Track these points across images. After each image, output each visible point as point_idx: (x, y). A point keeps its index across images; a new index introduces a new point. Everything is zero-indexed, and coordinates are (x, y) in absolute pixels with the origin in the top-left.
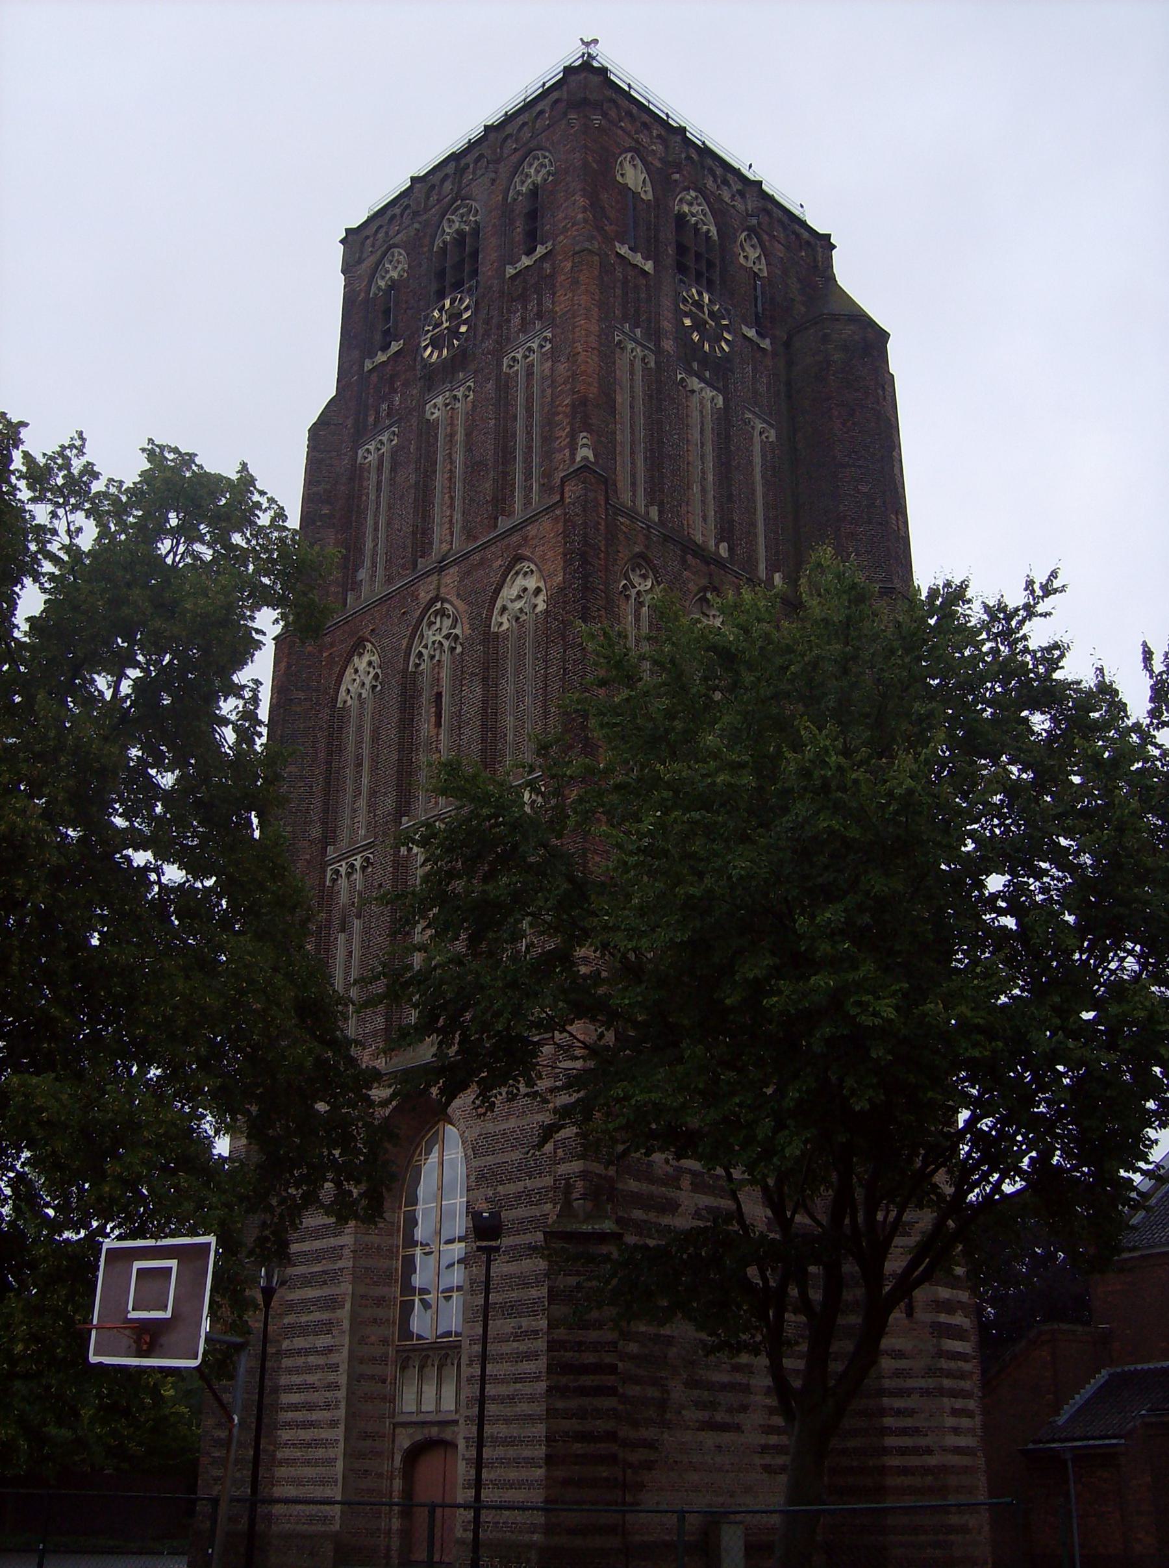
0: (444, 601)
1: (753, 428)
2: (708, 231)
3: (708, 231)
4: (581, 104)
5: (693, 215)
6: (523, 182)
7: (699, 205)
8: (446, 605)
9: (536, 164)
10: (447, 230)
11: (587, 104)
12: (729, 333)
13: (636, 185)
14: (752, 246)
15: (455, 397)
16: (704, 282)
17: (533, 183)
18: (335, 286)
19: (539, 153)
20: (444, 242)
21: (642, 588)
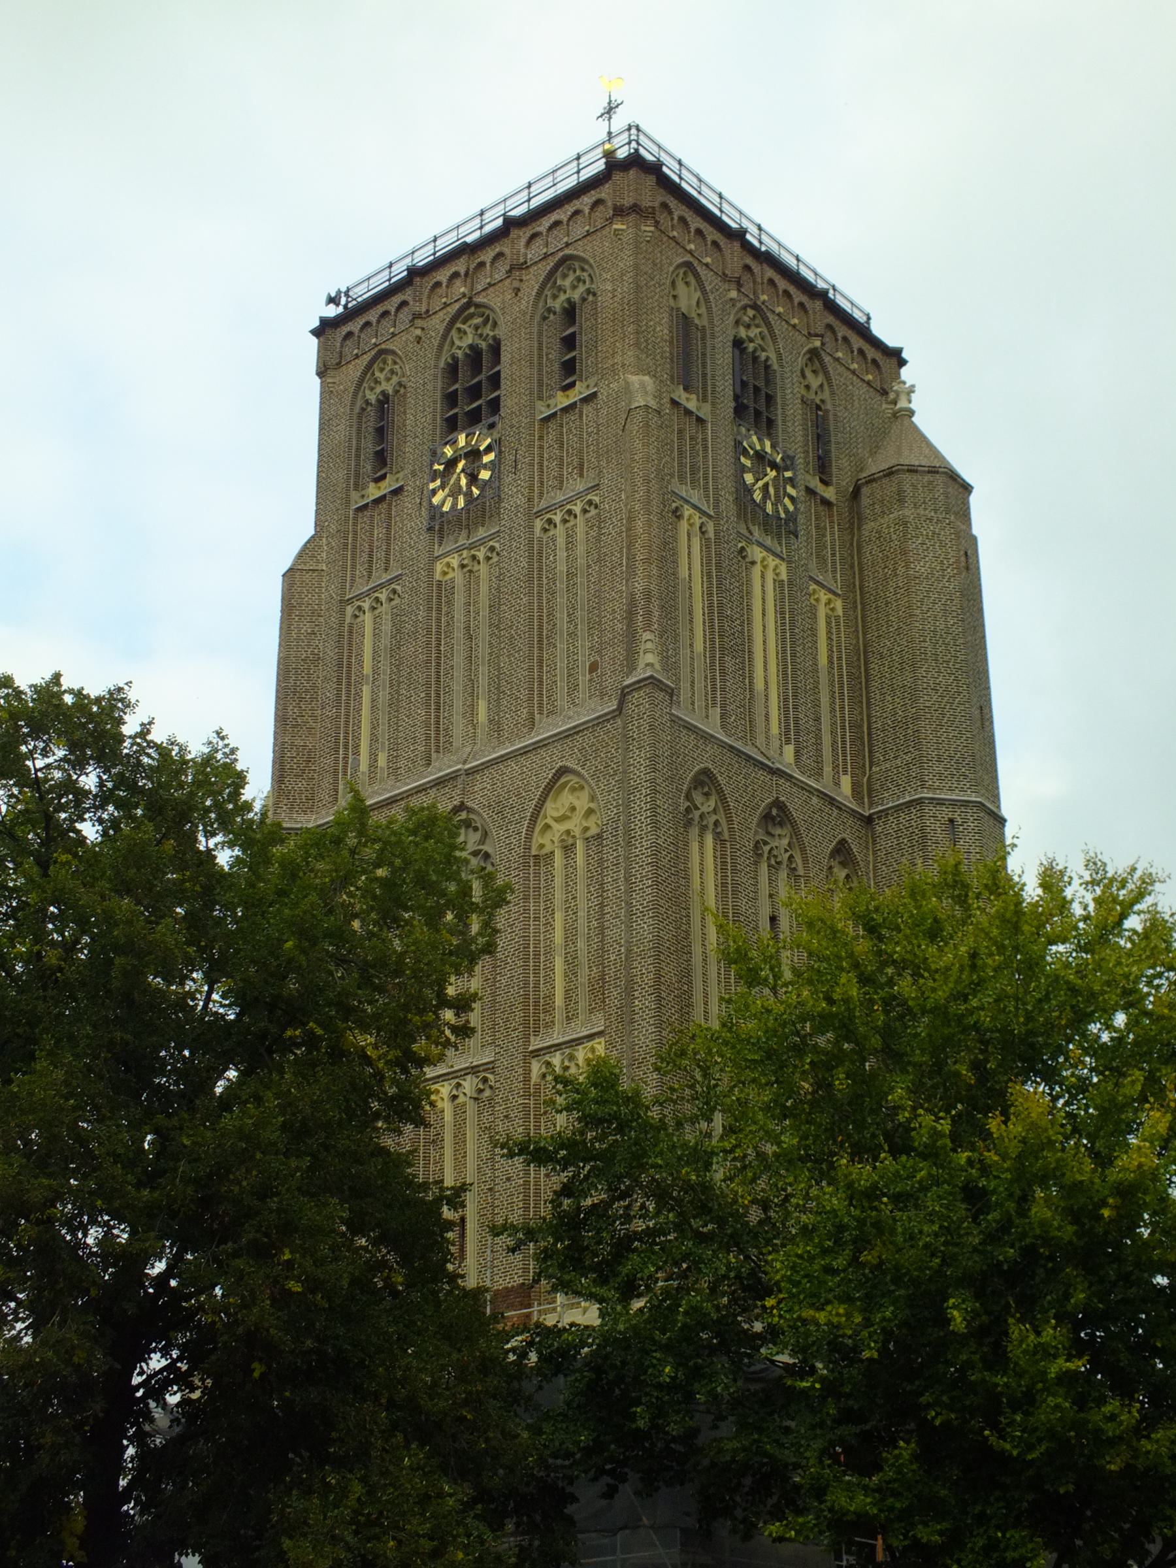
0: (470, 810)
1: (817, 600)
2: (768, 358)
3: (768, 358)
4: (629, 188)
5: (751, 340)
6: (555, 297)
7: (757, 326)
8: (472, 816)
9: (571, 277)
10: (457, 343)
11: (636, 189)
12: (793, 486)
13: (689, 306)
14: (814, 372)
15: (474, 557)
16: (764, 425)
17: (569, 300)
18: (272, 755)
19: (577, 264)
20: (454, 357)
21: (704, 809)
